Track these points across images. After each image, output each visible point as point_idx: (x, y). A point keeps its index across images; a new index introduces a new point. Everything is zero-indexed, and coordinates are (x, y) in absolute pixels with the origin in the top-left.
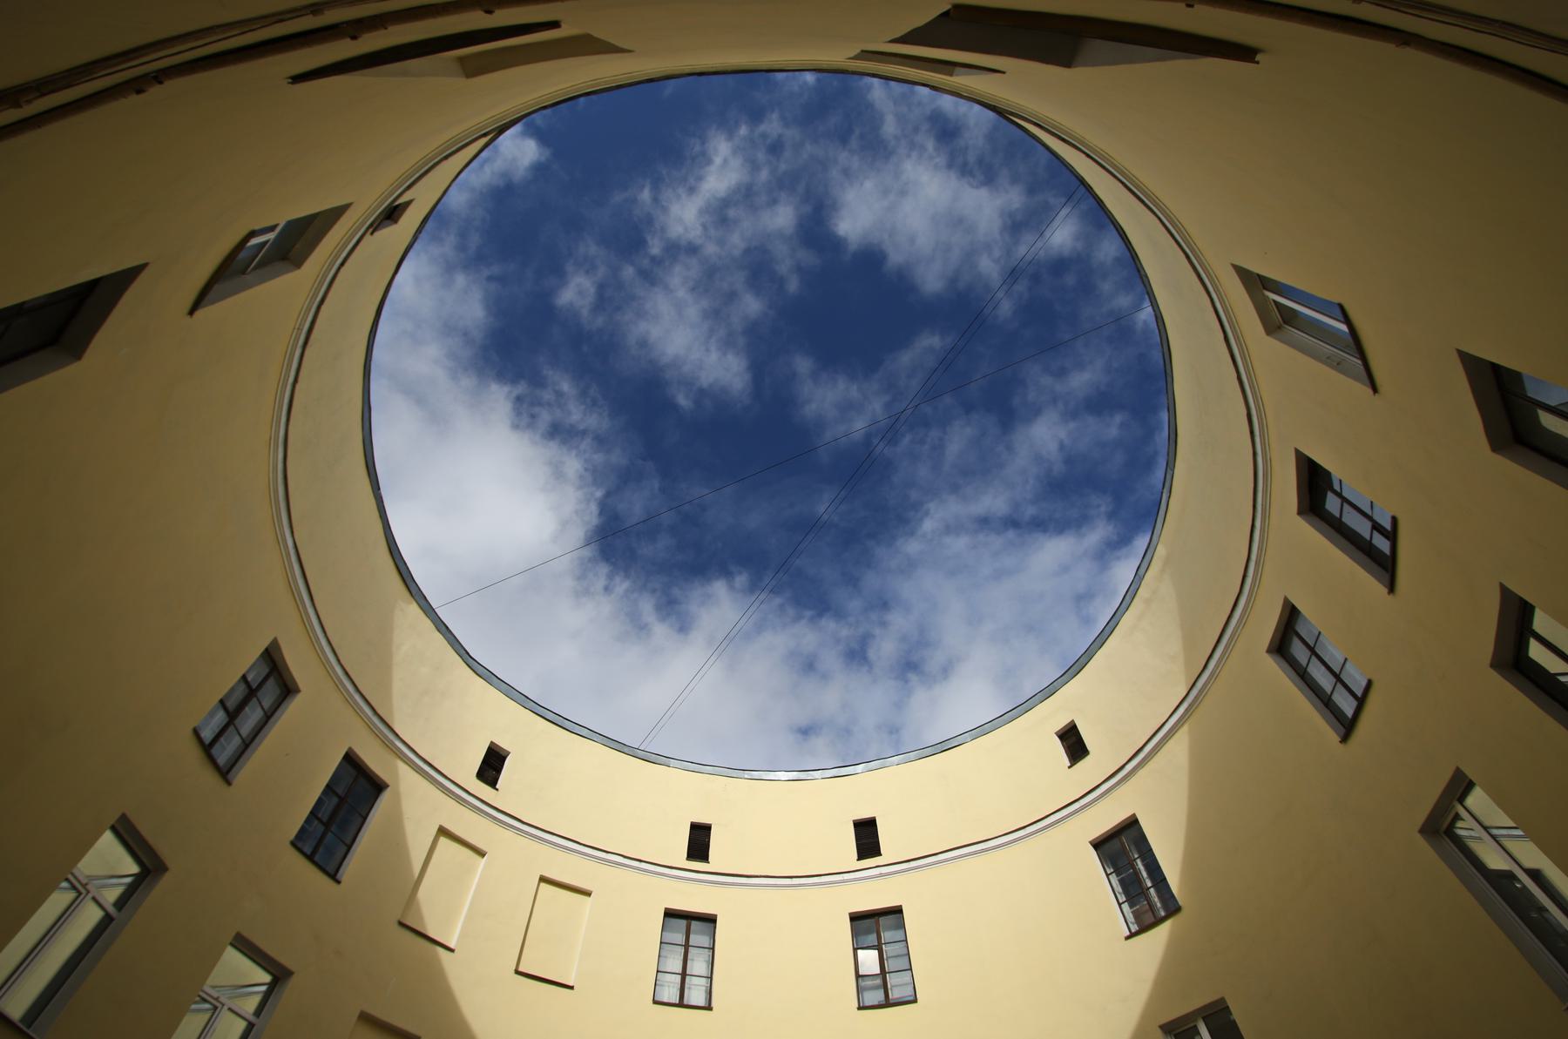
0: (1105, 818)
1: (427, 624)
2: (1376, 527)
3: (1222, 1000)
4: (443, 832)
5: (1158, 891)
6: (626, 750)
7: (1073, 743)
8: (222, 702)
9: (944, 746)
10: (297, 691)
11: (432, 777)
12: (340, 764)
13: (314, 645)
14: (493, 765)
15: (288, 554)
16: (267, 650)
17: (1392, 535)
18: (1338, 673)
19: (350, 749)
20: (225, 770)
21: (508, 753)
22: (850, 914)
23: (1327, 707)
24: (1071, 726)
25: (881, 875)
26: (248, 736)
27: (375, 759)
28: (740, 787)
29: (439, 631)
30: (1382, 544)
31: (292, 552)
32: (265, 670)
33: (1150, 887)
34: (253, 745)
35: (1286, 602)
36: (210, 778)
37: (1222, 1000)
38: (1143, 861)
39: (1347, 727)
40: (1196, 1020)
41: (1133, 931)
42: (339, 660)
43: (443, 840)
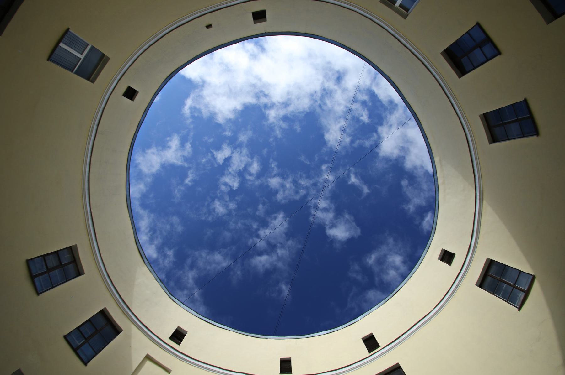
13: (99, 270)
14: (130, 94)
25: (383, 354)
43: (148, 363)
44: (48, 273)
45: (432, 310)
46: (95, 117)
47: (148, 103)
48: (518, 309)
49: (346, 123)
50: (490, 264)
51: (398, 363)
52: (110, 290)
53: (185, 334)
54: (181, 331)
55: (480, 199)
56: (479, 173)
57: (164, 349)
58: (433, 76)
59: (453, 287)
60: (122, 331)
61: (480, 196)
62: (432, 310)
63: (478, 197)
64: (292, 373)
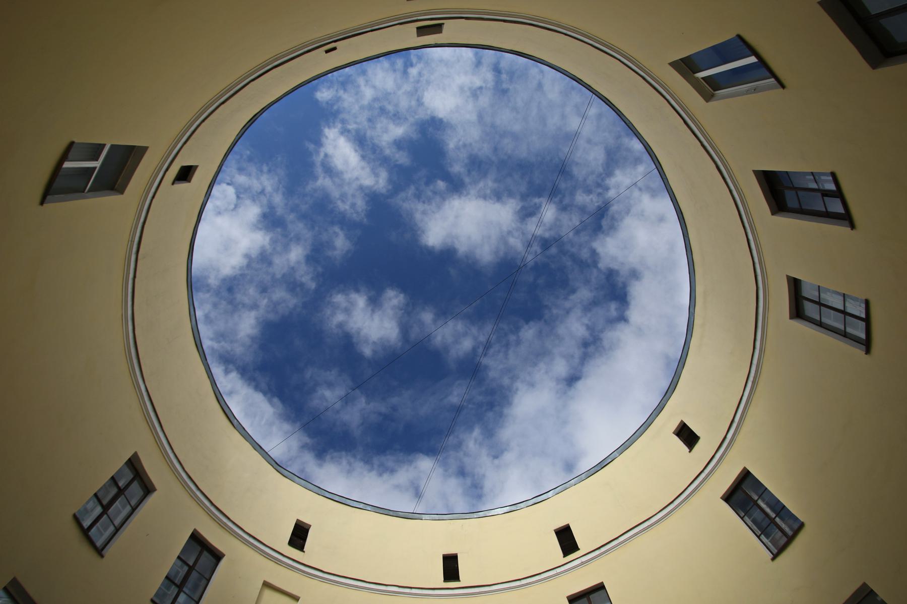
0: (726, 478)
1: (247, 445)
2: (826, 194)
3: (864, 585)
4: (267, 585)
7: (687, 435)
8: (96, 495)
9: (602, 465)
10: (154, 490)
11: (252, 544)
12: (188, 541)
13: (174, 473)
16: (130, 459)
19: (195, 530)
20: (100, 548)
21: (310, 526)
23: (846, 337)
24: (682, 425)
25: (583, 563)
27: (215, 537)
28: (471, 525)
29: (255, 449)
30: (836, 206)
33: (775, 518)
34: (121, 530)
36: (87, 552)
37: (864, 585)
38: (763, 500)
39: (867, 344)
40: (697, 78)
41: (774, 553)
42: (183, 469)
43: (268, 593)
44: (107, 514)
45: (655, 515)
47: (215, 172)
48: (772, 556)
49: (559, 177)
50: (746, 475)
52: (195, 498)
53: (307, 528)
55: (753, 382)
57: (284, 565)
60: (223, 555)
61: (755, 378)
62: (655, 515)
63: (751, 379)
64: (460, 581)
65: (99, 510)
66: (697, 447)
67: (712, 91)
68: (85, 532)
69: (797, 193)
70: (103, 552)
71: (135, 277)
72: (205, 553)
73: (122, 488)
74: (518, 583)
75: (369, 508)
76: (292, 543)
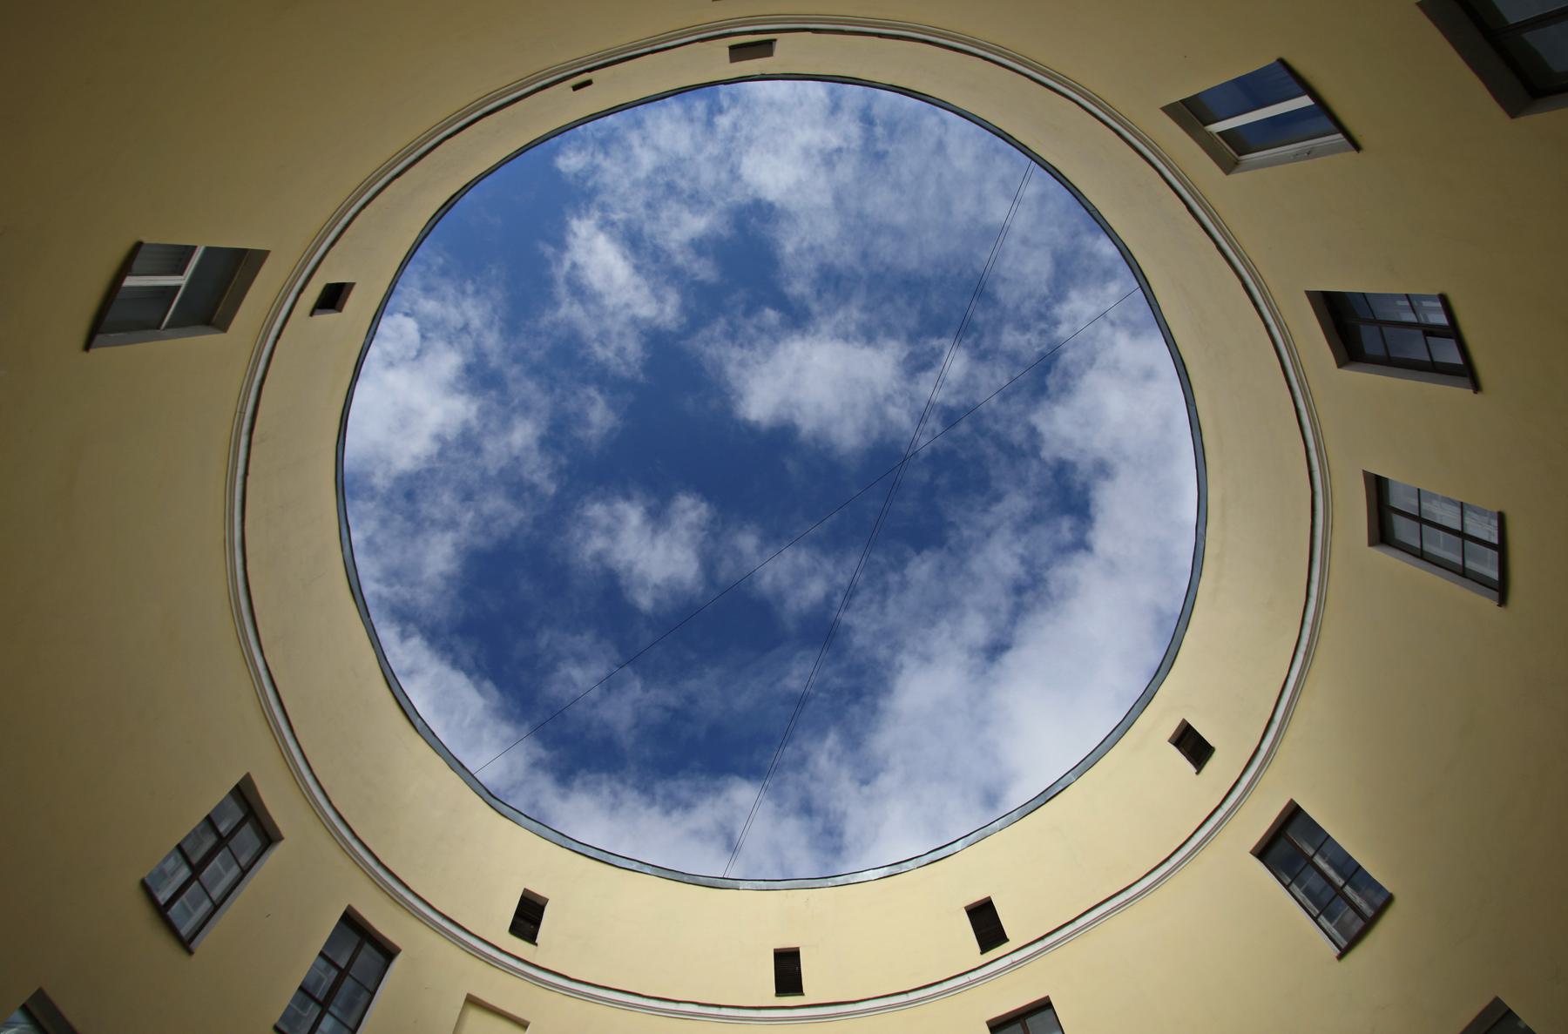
0: (1259, 818)
4: (472, 1001)
5: (1356, 888)
6: (686, 878)
7: (1193, 746)
9: (1047, 796)
14: (529, 916)
15: (258, 676)
16: (237, 787)
17: (1452, 331)
18: (1460, 529)
19: (350, 908)
20: (187, 939)
21: (546, 900)
22: (988, 1023)
23: (1466, 577)
24: (1184, 727)
25: (1014, 964)
26: (218, 899)
27: (384, 919)
31: (263, 674)
32: (239, 815)
34: (223, 907)
35: (1367, 475)
38: (1323, 856)
41: (1343, 946)
42: (330, 802)
45: (1139, 881)
46: (240, 412)
48: (1338, 951)
50: (1293, 813)
51: (1048, 996)
53: (541, 903)
54: (530, 897)
55: (1307, 654)
56: (1322, 591)
58: (1263, 325)
59: (1196, 836)
61: (1309, 646)
62: (1139, 881)
63: (1303, 648)
64: (803, 994)
65: (185, 872)
66: (1211, 765)
67: (1236, 156)
68: (162, 911)
69: (1421, 526)
70: (193, 945)
71: (246, 473)
72: (367, 947)
73: (225, 836)
74: (903, 998)
75: (647, 869)
76: (515, 929)
